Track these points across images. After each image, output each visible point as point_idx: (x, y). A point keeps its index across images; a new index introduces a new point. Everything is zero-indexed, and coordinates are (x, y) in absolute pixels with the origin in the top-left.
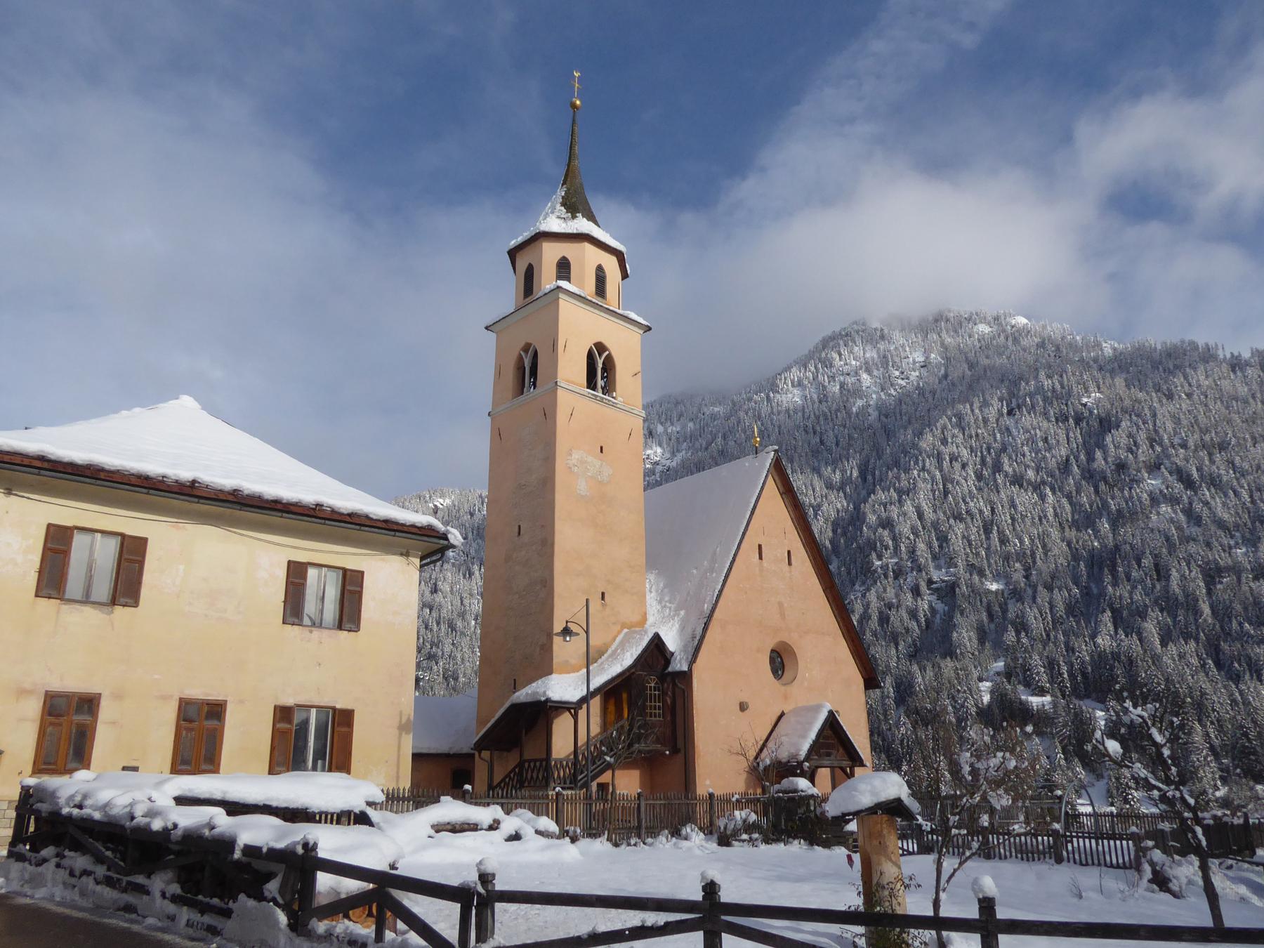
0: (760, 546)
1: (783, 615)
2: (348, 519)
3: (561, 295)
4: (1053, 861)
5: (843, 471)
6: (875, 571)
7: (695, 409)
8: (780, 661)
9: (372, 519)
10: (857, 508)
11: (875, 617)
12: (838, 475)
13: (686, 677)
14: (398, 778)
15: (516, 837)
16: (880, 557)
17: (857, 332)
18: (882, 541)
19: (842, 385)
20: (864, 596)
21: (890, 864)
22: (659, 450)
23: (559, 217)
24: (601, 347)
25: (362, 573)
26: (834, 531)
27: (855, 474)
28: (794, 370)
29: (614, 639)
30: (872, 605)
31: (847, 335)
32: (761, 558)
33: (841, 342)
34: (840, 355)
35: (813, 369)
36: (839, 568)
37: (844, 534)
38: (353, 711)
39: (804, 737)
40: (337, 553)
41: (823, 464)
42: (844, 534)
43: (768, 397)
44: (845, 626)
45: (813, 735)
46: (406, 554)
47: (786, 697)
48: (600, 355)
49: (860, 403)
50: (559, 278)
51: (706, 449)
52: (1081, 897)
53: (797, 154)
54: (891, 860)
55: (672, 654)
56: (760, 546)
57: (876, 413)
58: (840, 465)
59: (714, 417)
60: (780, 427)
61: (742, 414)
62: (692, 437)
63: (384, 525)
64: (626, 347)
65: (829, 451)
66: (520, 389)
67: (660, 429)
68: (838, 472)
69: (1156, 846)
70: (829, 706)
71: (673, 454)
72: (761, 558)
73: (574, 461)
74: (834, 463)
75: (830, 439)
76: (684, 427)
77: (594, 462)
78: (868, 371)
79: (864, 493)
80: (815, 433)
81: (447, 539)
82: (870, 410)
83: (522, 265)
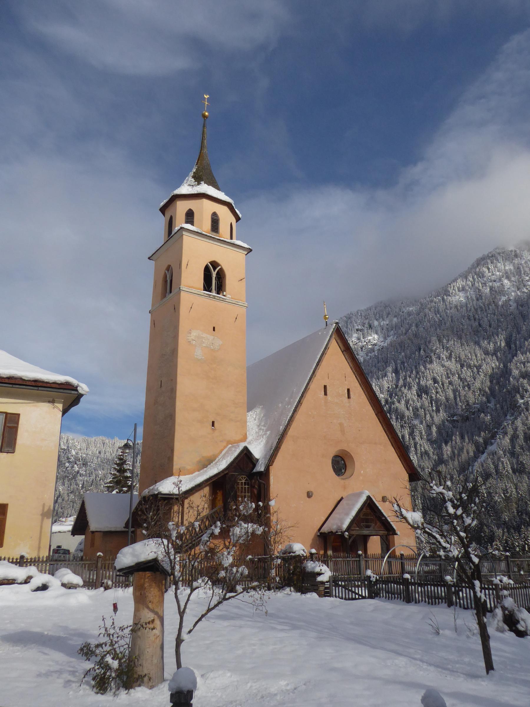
0: (325, 387)
1: (343, 432)
2: (7, 381)
3: (184, 233)
4: (446, 605)
5: (495, 343)
6: (520, 406)
7: (397, 310)
8: (341, 464)
9: (24, 380)
10: (505, 366)
11: (521, 437)
12: (492, 346)
13: (265, 475)
14: (39, 548)
15: (44, 587)
16: (522, 397)
17: (499, 254)
18: (523, 387)
19: (491, 288)
20: (513, 423)
21: (146, 611)
22: (376, 336)
23: (189, 185)
24: (215, 264)
25: (18, 415)
26: (491, 382)
27: (503, 344)
28: (459, 281)
29: (221, 452)
31: (492, 256)
32: (326, 394)
33: (489, 261)
34: (489, 269)
35: (471, 279)
36: (495, 405)
37: (498, 383)
38: (7, 505)
39: (347, 514)
40: (7, 403)
41: (481, 339)
42: (498, 383)
43: (443, 299)
44: (393, 437)
45: (353, 513)
46: (53, 402)
47: (345, 488)
48: (214, 271)
49: (504, 298)
50: (187, 222)
51: (406, 334)
52: (438, 633)
53: (451, 146)
54: (148, 608)
55: (257, 460)
56: (325, 387)
57: (515, 305)
58: (493, 339)
59: (409, 314)
60: (452, 317)
61: (427, 311)
62: (396, 327)
63: (33, 384)
64: (232, 262)
65: (485, 331)
66: (164, 295)
67: (376, 323)
68: (491, 344)
70: (367, 493)
71: (385, 338)
72: (326, 394)
73: (193, 337)
74: (489, 338)
75: (485, 323)
76: (391, 321)
77: (208, 337)
78: (508, 278)
79: (510, 356)
80: (475, 319)
81: (77, 390)
82: (511, 303)
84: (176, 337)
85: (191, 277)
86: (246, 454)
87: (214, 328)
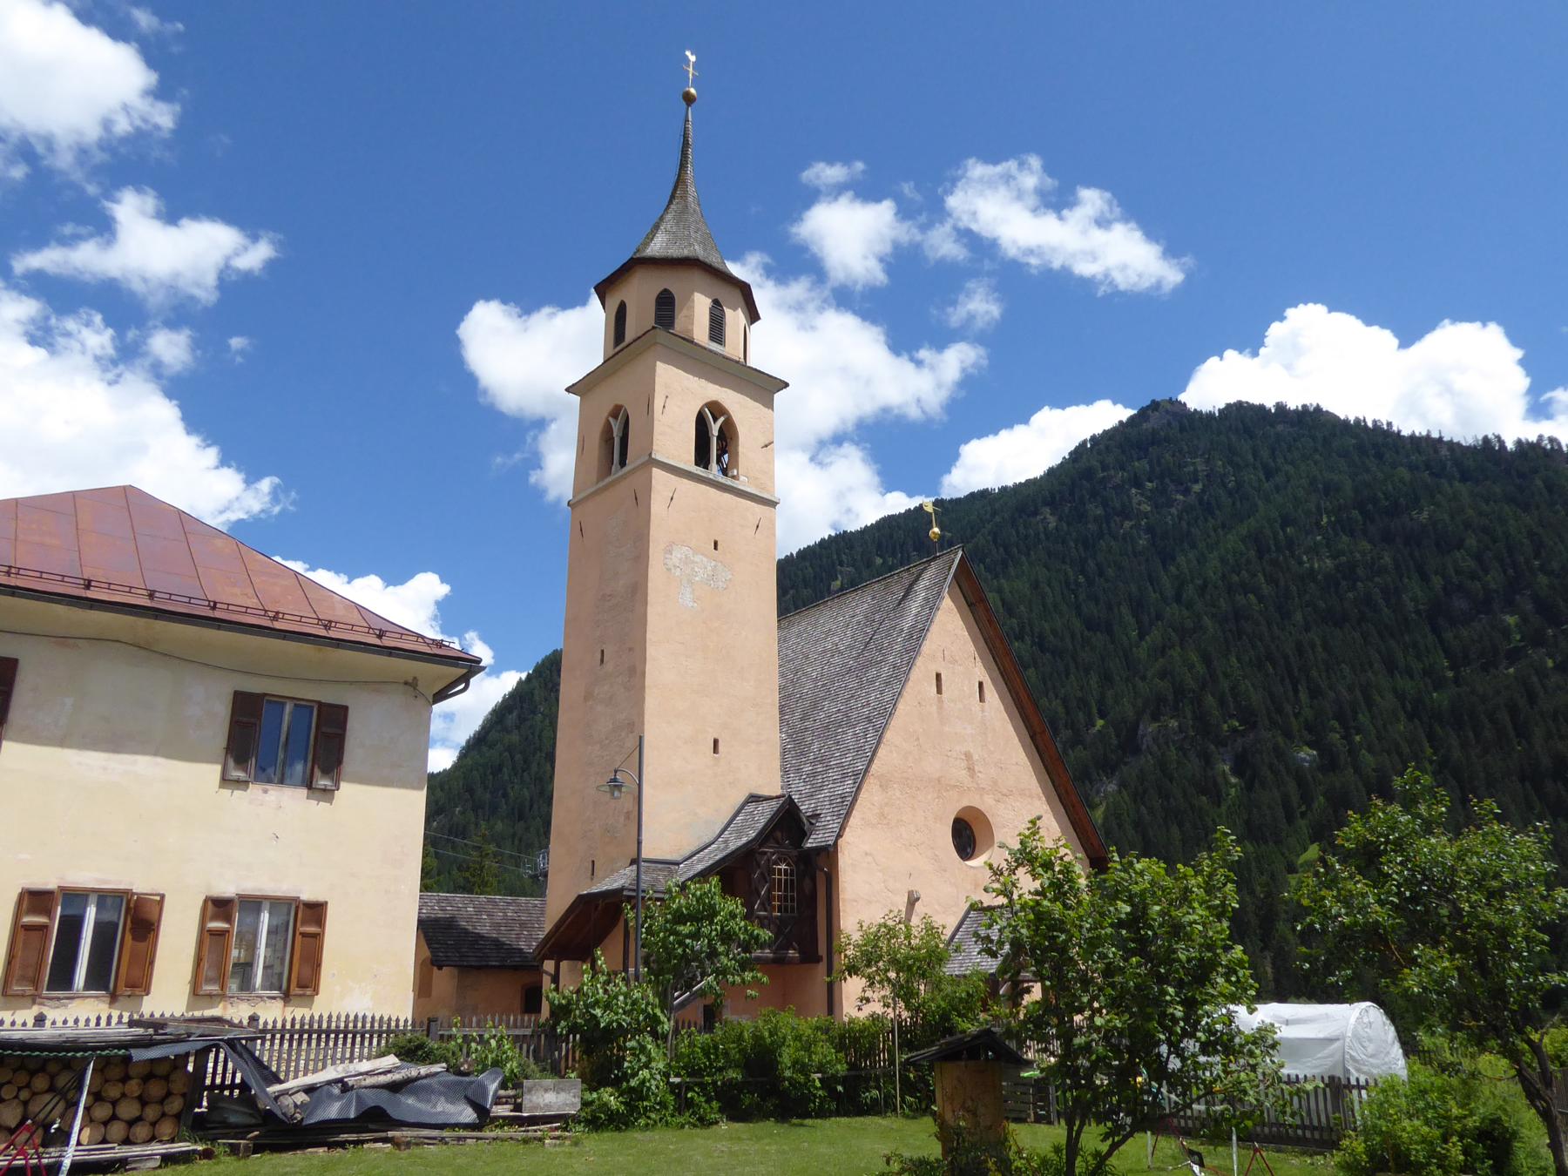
0: (938, 676)
25: (346, 708)
32: (939, 691)
48: (715, 420)
56: (938, 676)
69: (1117, 1136)
72: (939, 691)
83: (614, 303)
84: (641, 558)
85: (673, 437)
86: (788, 811)
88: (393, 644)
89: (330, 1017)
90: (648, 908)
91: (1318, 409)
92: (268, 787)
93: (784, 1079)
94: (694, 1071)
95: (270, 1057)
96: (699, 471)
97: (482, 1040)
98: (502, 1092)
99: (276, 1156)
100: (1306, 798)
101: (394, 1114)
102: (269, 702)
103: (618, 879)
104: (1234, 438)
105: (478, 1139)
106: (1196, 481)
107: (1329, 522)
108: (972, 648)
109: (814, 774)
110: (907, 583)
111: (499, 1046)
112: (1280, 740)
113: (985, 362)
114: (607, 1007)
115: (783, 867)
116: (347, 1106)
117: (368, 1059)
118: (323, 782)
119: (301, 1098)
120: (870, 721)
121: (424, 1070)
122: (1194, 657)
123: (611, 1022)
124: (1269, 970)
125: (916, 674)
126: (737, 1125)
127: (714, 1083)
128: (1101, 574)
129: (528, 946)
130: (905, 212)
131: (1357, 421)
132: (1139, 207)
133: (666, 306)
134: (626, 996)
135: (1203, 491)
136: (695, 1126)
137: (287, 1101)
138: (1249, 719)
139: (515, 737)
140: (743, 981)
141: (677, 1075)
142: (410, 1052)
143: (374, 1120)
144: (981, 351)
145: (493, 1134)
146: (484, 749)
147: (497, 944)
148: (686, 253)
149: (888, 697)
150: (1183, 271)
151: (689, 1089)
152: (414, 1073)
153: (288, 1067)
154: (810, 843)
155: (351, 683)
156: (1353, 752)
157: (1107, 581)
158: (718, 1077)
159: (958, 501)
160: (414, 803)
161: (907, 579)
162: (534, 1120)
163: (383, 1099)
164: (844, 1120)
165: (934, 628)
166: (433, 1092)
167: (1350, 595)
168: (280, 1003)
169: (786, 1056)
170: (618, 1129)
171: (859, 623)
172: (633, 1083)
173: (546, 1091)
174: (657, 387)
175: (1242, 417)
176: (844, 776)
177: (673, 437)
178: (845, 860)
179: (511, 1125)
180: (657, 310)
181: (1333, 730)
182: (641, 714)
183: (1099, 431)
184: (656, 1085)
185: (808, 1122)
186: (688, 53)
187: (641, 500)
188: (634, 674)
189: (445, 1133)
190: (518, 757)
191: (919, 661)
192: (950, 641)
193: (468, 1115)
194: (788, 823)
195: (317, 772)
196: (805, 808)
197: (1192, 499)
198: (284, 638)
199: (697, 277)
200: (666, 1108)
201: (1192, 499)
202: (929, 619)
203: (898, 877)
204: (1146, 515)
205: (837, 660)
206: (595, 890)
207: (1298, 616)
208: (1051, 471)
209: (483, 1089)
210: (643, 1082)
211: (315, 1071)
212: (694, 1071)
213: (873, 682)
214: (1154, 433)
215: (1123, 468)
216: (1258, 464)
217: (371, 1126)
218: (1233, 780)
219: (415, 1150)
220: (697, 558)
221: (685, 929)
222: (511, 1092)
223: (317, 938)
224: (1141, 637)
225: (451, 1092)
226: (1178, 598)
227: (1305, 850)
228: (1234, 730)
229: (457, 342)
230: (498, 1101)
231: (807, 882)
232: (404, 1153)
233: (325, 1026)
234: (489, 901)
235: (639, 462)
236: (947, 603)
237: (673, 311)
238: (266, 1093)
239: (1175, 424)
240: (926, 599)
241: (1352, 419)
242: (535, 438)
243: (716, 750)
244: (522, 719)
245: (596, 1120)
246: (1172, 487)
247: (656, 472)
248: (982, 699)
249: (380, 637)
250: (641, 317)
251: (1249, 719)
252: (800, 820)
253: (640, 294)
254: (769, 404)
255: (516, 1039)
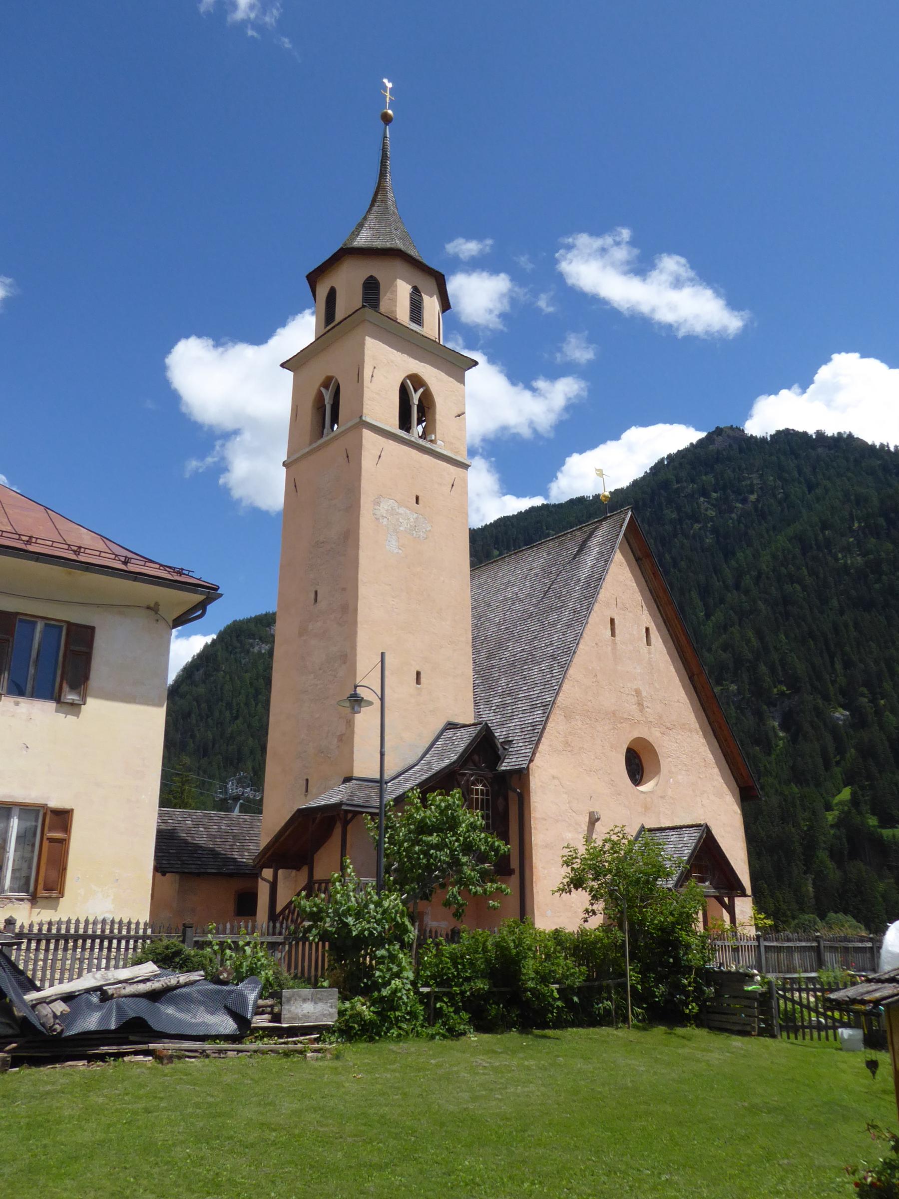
0: (612, 621)
25: (92, 629)
30: (286, 969)
32: (613, 634)
38: (72, 810)
48: (416, 391)
56: (612, 621)
72: (613, 634)
83: (322, 291)
84: (352, 508)
85: (380, 403)
87: (417, 498)
88: (138, 570)
89: (78, 921)
90: (389, 818)
91: (850, 436)
92: (19, 699)
93: (526, 990)
94: (441, 979)
95: (34, 970)
96: (402, 434)
97: (236, 948)
98: (260, 1002)
99: (34, 1069)
100: (841, 750)
101: (156, 1026)
102: (21, 621)
103: (334, 795)
104: (782, 458)
105: (239, 1051)
106: (752, 493)
107: (860, 526)
108: (640, 598)
109: (504, 705)
110: (580, 540)
111: (254, 953)
112: (820, 701)
113: (585, 394)
114: (359, 915)
115: (480, 787)
116: (105, 1019)
117: (124, 967)
118: (71, 697)
119: (60, 1007)
120: (555, 659)
121: (183, 978)
122: (750, 634)
123: (363, 930)
124: (811, 889)
125: (594, 618)
126: (486, 1037)
127: (463, 993)
128: (675, 564)
129: (246, 858)
130: (517, 276)
131: (882, 445)
132: (707, 272)
133: (372, 291)
134: (378, 904)
135: (758, 500)
136: (444, 1037)
137: (45, 1010)
138: (794, 685)
139: (201, 690)
140: (485, 891)
141: (426, 985)
142: (168, 960)
143: (135, 1032)
144: (583, 384)
145: (253, 1047)
146: (177, 698)
147: (214, 854)
148: (388, 245)
149: (570, 637)
150: (743, 320)
151: (438, 998)
152: (173, 981)
153: (44, 975)
154: (504, 767)
155: (98, 605)
156: (878, 712)
157: (680, 571)
158: (466, 987)
159: (560, 505)
160: (151, 722)
161: (579, 536)
162: (292, 1032)
163: (141, 1009)
164: (581, 1031)
165: (609, 578)
166: (192, 1001)
167: (877, 586)
168: (26, 905)
169: (529, 967)
170: (371, 1040)
171: (536, 575)
172: (385, 992)
173: (305, 1000)
174: (366, 358)
175: (789, 441)
176: (534, 707)
177: (380, 403)
178: (536, 781)
179: (270, 1036)
180: (364, 293)
181: (863, 695)
182: (354, 647)
183: (674, 451)
184: (407, 997)
185: (549, 1032)
186: (385, 81)
187: (352, 457)
188: (347, 612)
189: (207, 1046)
190: (204, 705)
191: (596, 607)
192: (621, 590)
193: (228, 1025)
194: (485, 748)
195: (66, 688)
196: (499, 734)
197: (749, 507)
198: (37, 560)
199: (399, 266)
200: (417, 1018)
201: (749, 507)
202: (605, 570)
203: (574, 802)
204: (711, 519)
205: (517, 606)
206: (313, 804)
207: (835, 603)
208: (635, 483)
209: (243, 998)
210: (395, 992)
211: (70, 979)
212: (441, 979)
213: (554, 625)
214: (718, 452)
215: (693, 481)
216: (802, 479)
217: (132, 1038)
218: (781, 734)
219: (178, 1065)
220: (402, 510)
221: (434, 839)
222: (269, 1002)
223: (62, 844)
224: (708, 616)
225: (213, 1002)
226: (737, 587)
227: (839, 792)
228: (782, 694)
229: (164, 368)
230: (259, 1010)
231: (501, 801)
232: (168, 1068)
233: (81, 931)
234: (205, 815)
235: (349, 424)
236: (618, 557)
237: (378, 294)
238: (23, 1002)
239: (735, 446)
240: (601, 553)
241: (878, 444)
242: (223, 445)
243: (418, 681)
244: (207, 675)
245: (351, 1030)
246: (732, 497)
247: (366, 433)
248: (649, 643)
249: (125, 563)
250: (349, 299)
251: (794, 685)
252: (495, 745)
253: (348, 281)
254: (462, 380)
255: (273, 946)
